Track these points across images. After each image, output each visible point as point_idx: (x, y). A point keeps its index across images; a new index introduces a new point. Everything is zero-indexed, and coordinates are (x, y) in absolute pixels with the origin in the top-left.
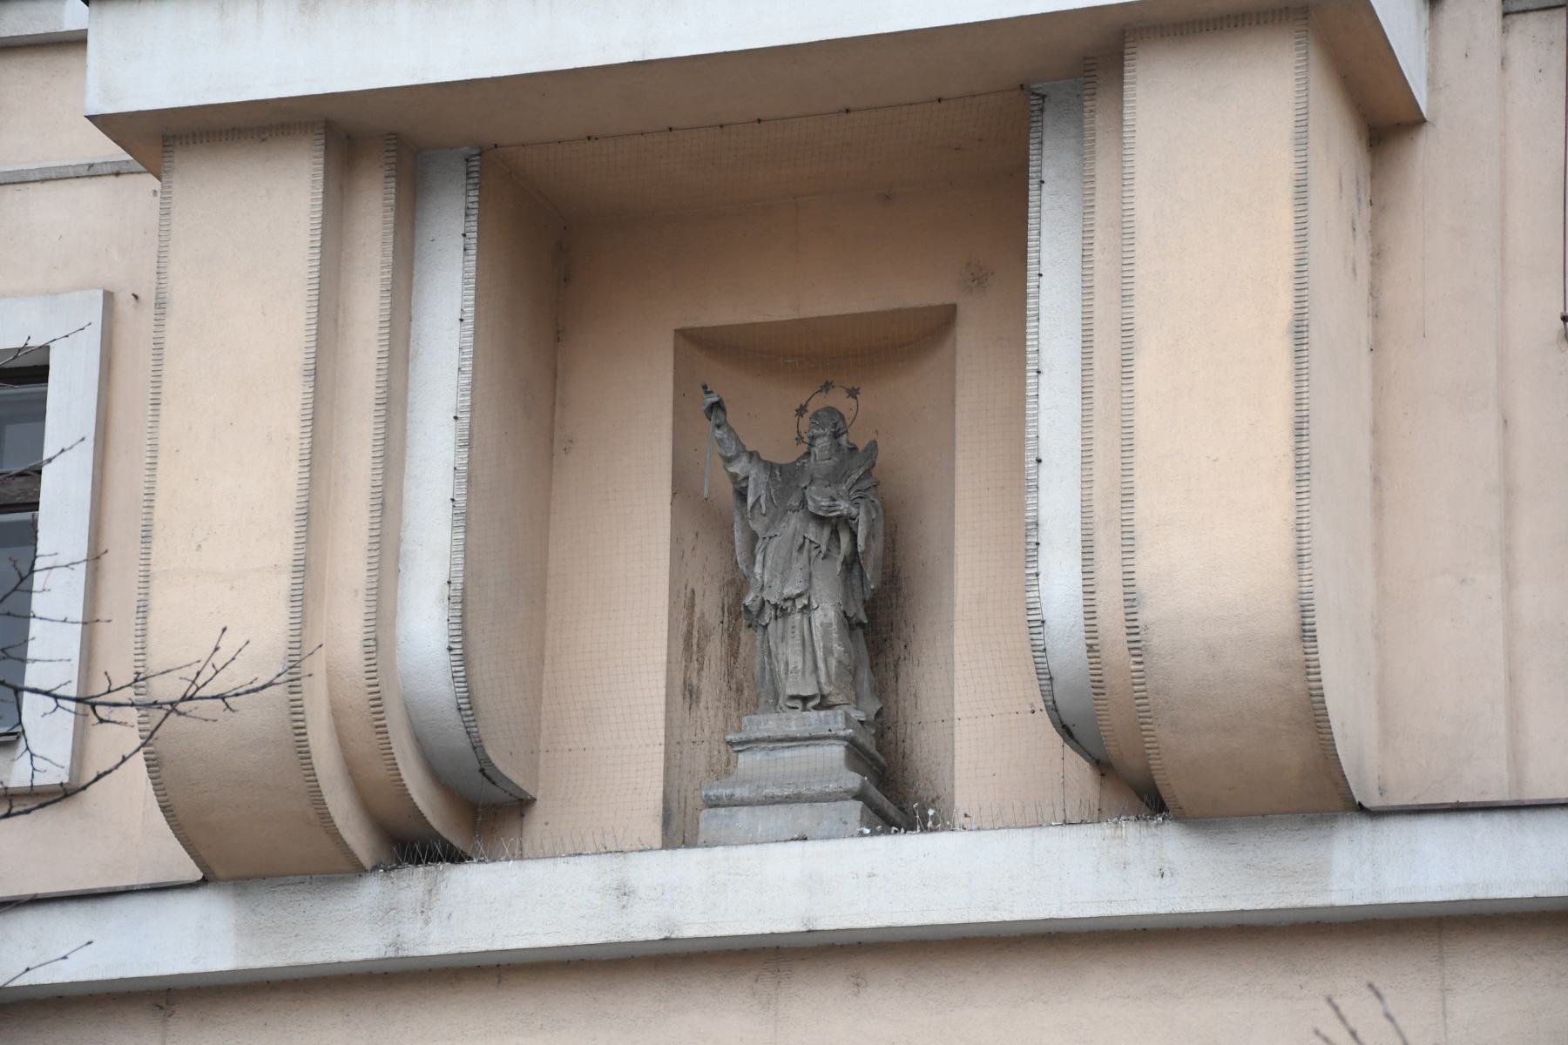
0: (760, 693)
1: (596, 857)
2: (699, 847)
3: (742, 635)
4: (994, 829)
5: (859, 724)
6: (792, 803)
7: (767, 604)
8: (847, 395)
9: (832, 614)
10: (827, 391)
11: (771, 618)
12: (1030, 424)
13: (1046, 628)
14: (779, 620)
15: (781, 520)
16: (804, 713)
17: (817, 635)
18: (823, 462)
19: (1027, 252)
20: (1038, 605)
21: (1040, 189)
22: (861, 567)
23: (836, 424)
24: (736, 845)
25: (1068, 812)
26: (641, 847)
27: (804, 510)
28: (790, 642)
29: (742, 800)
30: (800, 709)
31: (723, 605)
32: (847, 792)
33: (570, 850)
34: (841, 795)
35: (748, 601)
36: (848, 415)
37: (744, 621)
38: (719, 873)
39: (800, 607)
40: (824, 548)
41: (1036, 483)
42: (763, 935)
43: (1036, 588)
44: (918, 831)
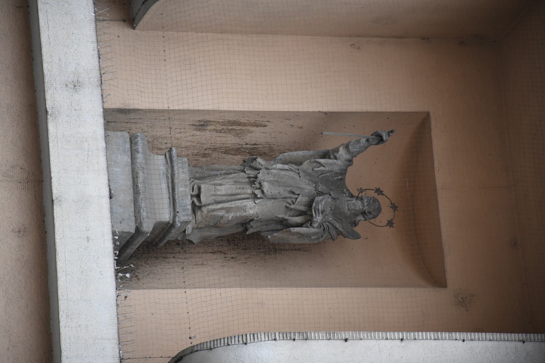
0: (203, 168)
1: (97, 68)
2: (105, 132)
3: (239, 156)
4: (118, 315)
5: (183, 230)
6: (133, 189)
7: (258, 172)
8: (389, 220)
9: (251, 212)
10: (391, 207)
11: (248, 174)
12: (369, 334)
13: (242, 345)
14: (247, 180)
15: (310, 180)
16: (190, 196)
17: (239, 203)
18: (346, 206)
19: (479, 332)
20: (256, 340)
21: (519, 341)
22: (281, 230)
23: (370, 213)
24: (106, 155)
25: (128, 361)
26: (104, 96)
27: (316, 194)
28: (234, 187)
29: (135, 158)
30: (193, 193)
31: (258, 145)
32: (141, 223)
33: (102, 51)
34: (138, 220)
35: (259, 160)
36: (377, 221)
37: (248, 158)
38: (89, 144)
39: (255, 192)
40: (292, 206)
41: (332, 338)
42: (50, 172)
43: (267, 339)
44: (116, 268)
